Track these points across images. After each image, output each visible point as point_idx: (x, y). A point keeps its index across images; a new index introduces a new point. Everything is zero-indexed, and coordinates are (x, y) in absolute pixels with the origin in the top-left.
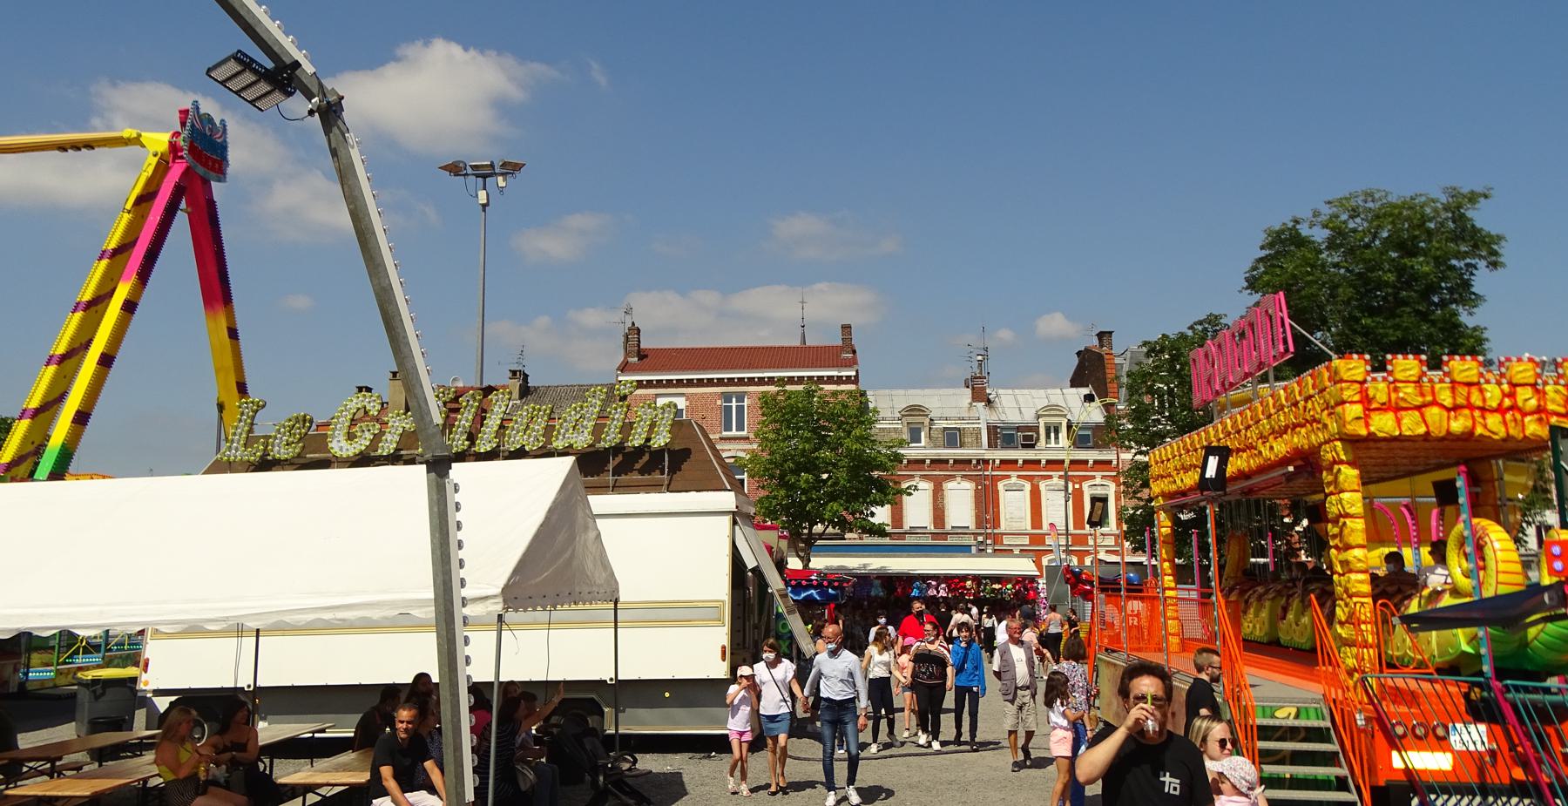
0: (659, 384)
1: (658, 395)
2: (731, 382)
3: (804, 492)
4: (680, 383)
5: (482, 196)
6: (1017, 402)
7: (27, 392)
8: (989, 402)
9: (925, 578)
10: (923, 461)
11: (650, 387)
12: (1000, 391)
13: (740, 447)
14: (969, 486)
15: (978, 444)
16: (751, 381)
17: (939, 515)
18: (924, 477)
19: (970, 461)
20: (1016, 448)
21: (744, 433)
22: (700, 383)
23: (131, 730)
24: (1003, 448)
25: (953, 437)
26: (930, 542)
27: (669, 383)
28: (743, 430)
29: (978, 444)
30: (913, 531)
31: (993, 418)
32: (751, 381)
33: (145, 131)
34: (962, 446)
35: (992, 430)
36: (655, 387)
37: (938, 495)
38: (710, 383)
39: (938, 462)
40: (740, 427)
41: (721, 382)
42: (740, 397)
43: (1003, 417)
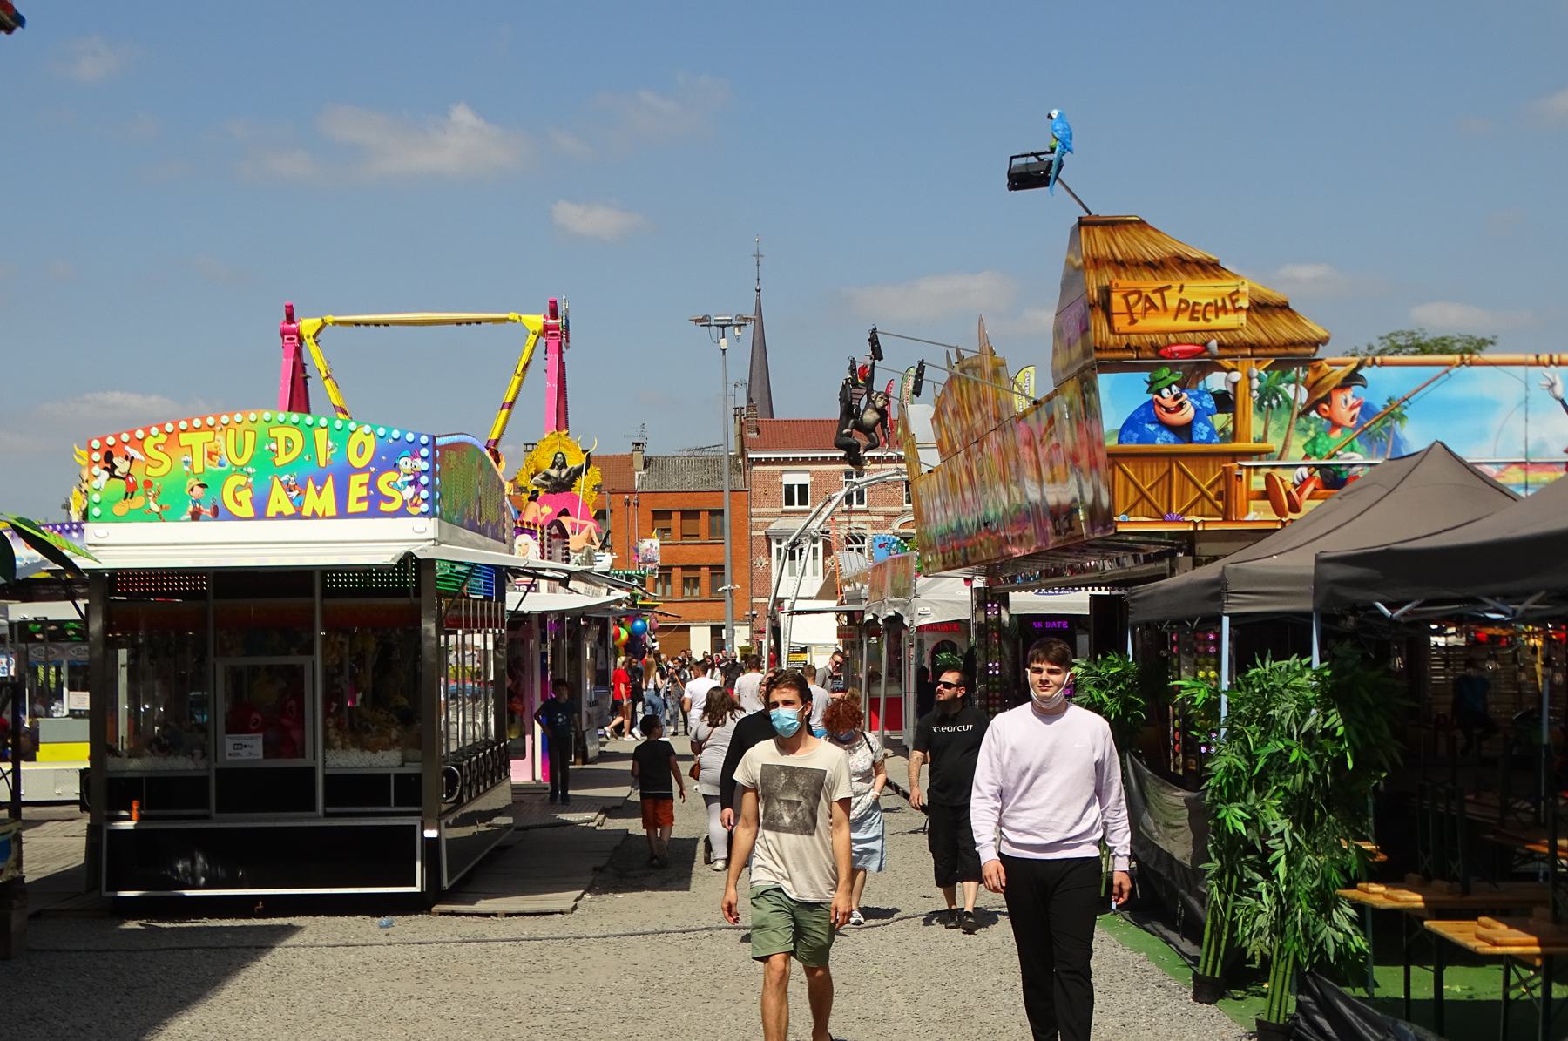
0: (786, 461)
1: (784, 471)
4: (805, 461)
7: (505, 390)
11: (777, 464)
13: (862, 519)
21: (864, 507)
23: (304, 757)
27: (795, 461)
28: (806, 504)
36: (782, 464)
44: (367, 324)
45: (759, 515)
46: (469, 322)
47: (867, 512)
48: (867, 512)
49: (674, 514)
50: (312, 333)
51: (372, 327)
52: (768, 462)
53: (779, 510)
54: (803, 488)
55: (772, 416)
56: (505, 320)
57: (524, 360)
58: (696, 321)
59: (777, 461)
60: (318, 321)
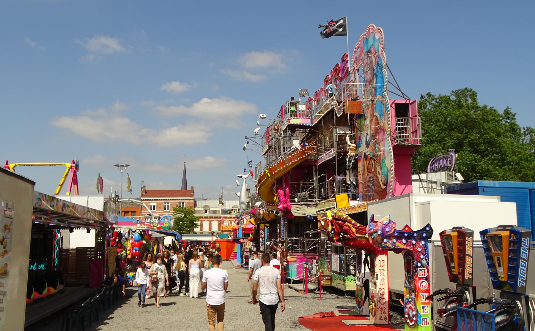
1: (150, 202)
2: (166, 200)
3: (181, 226)
5: (122, 171)
6: (229, 203)
8: (223, 204)
9: (204, 241)
10: (207, 217)
12: (226, 201)
14: (217, 222)
15: (219, 213)
16: (171, 200)
17: (210, 228)
18: (208, 220)
19: (217, 217)
20: (227, 214)
22: (159, 200)
24: (225, 214)
25: (214, 212)
26: (199, 234)
27: (153, 200)
29: (219, 213)
30: (205, 232)
31: (223, 208)
32: (171, 200)
33: (67, 163)
34: (216, 214)
35: (223, 210)
37: (210, 224)
38: (162, 200)
39: (211, 217)
40: (168, 209)
41: (164, 200)
42: (168, 203)
43: (225, 208)
44: (29, 165)
45: (143, 213)
46: (52, 165)
47: (169, 212)
48: (169, 212)
49: (129, 212)
50: (12, 167)
51: (28, 166)
52: (146, 200)
53: (163, 211)
54: (154, 207)
55: (187, 189)
56: (62, 165)
57: (65, 174)
58: (115, 165)
59: (148, 200)
60: (14, 165)
